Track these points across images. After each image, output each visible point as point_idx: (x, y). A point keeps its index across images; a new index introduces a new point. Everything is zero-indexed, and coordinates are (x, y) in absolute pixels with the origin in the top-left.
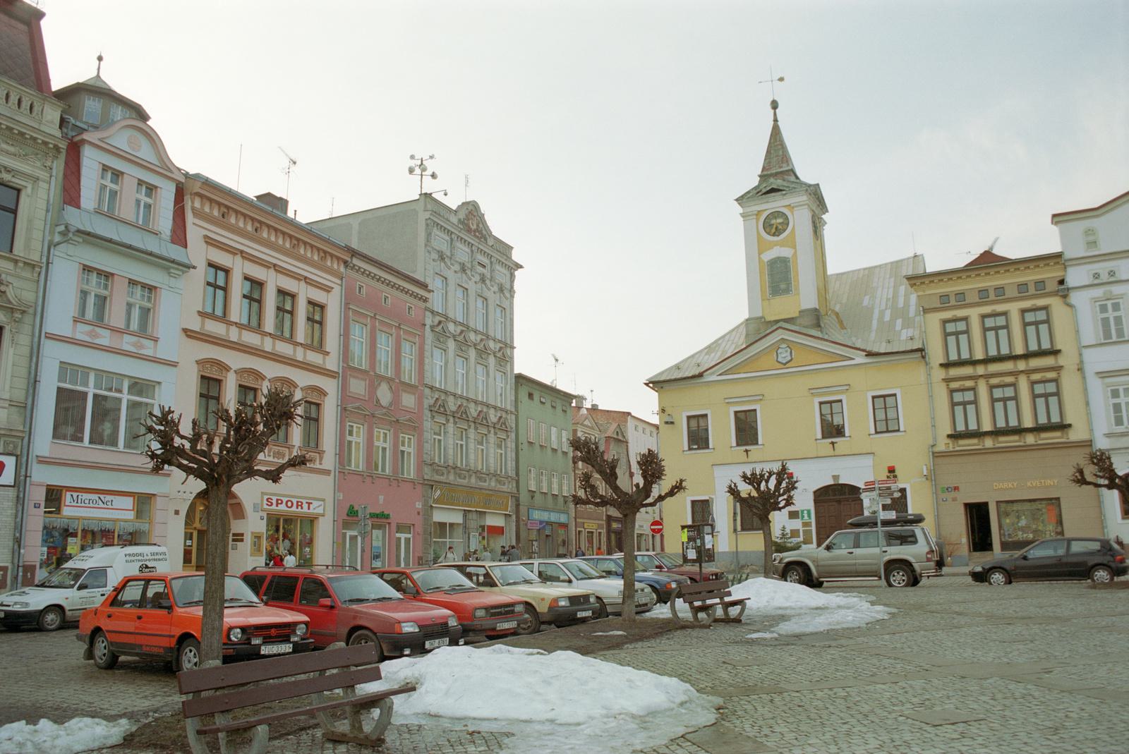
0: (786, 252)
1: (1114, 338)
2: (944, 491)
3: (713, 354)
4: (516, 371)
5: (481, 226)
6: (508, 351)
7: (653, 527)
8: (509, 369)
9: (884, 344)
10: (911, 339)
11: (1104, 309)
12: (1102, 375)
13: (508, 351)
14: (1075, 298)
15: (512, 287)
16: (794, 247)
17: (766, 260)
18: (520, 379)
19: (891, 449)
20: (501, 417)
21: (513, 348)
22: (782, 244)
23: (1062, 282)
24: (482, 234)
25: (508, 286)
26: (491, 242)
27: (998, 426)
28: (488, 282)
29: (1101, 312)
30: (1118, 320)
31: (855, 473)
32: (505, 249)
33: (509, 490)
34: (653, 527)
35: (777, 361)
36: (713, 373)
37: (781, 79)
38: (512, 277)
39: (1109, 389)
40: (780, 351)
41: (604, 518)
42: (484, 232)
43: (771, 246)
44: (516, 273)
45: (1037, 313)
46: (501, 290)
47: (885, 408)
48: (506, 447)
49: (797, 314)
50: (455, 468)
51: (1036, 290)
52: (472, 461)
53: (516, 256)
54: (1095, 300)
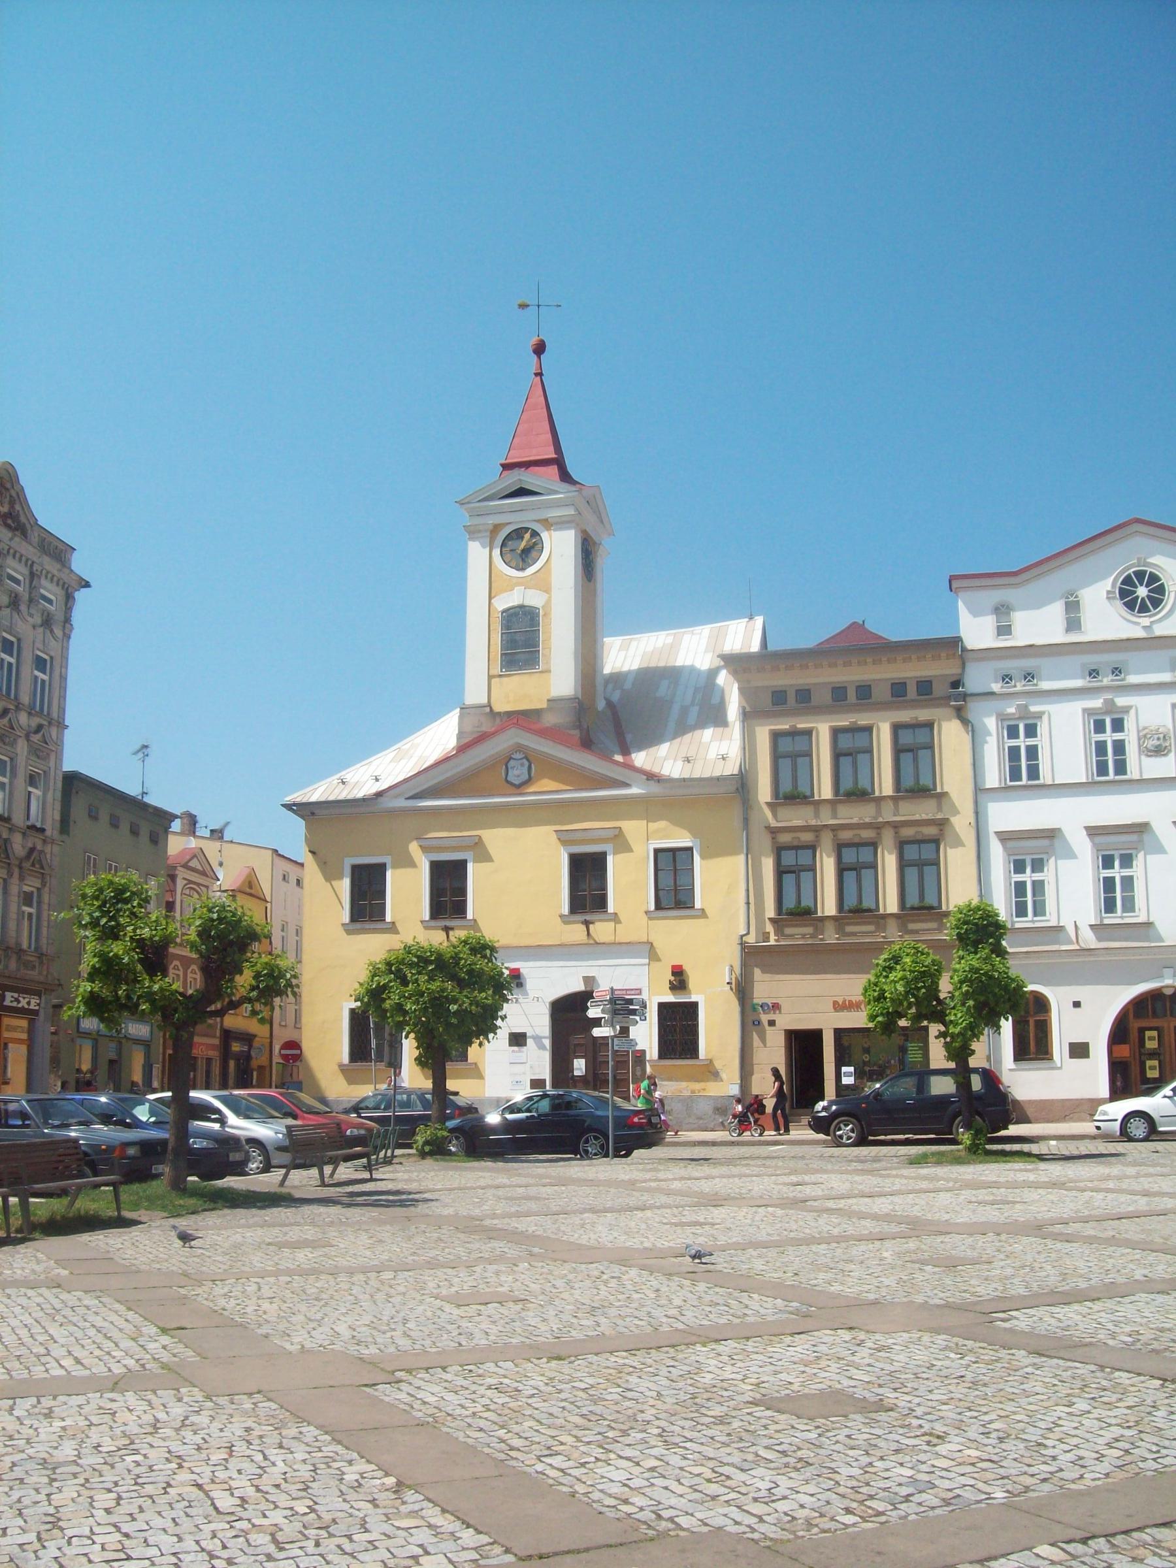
0: (534, 599)
1: (1024, 781)
2: (752, 1018)
3: (403, 762)
4: (68, 766)
5: (18, 507)
6: (54, 731)
7: (283, 1052)
8: (52, 764)
9: (680, 764)
10: (724, 759)
11: (1099, 727)
12: (1005, 837)
13: (54, 731)
14: (975, 709)
15: (67, 620)
16: (548, 590)
17: (500, 609)
18: (74, 782)
19: (676, 937)
20: (32, 850)
21: (61, 726)
22: (527, 584)
23: (956, 684)
24: (19, 522)
25: (59, 616)
26: (34, 537)
27: (803, 904)
28: (23, 608)
29: (1096, 732)
30: (1032, 752)
31: (614, 976)
32: (59, 552)
33: (42, 979)
34: (283, 1052)
35: (507, 782)
36: (397, 797)
37: (523, 306)
38: (69, 598)
39: (1012, 858)
40: (512, 763)
41: (218, 1034)
42: (23, 519)
43: (511, 585)
44: (77, 595)
45: (857, 735)
46: (47, 622)
47: (675, 870)
48: (39, 903)
49: (544, 705)
50: (20, 952)
51: (919, 695)
52: (12, 933)
53: (79, 564)
54: (1088, 712)
